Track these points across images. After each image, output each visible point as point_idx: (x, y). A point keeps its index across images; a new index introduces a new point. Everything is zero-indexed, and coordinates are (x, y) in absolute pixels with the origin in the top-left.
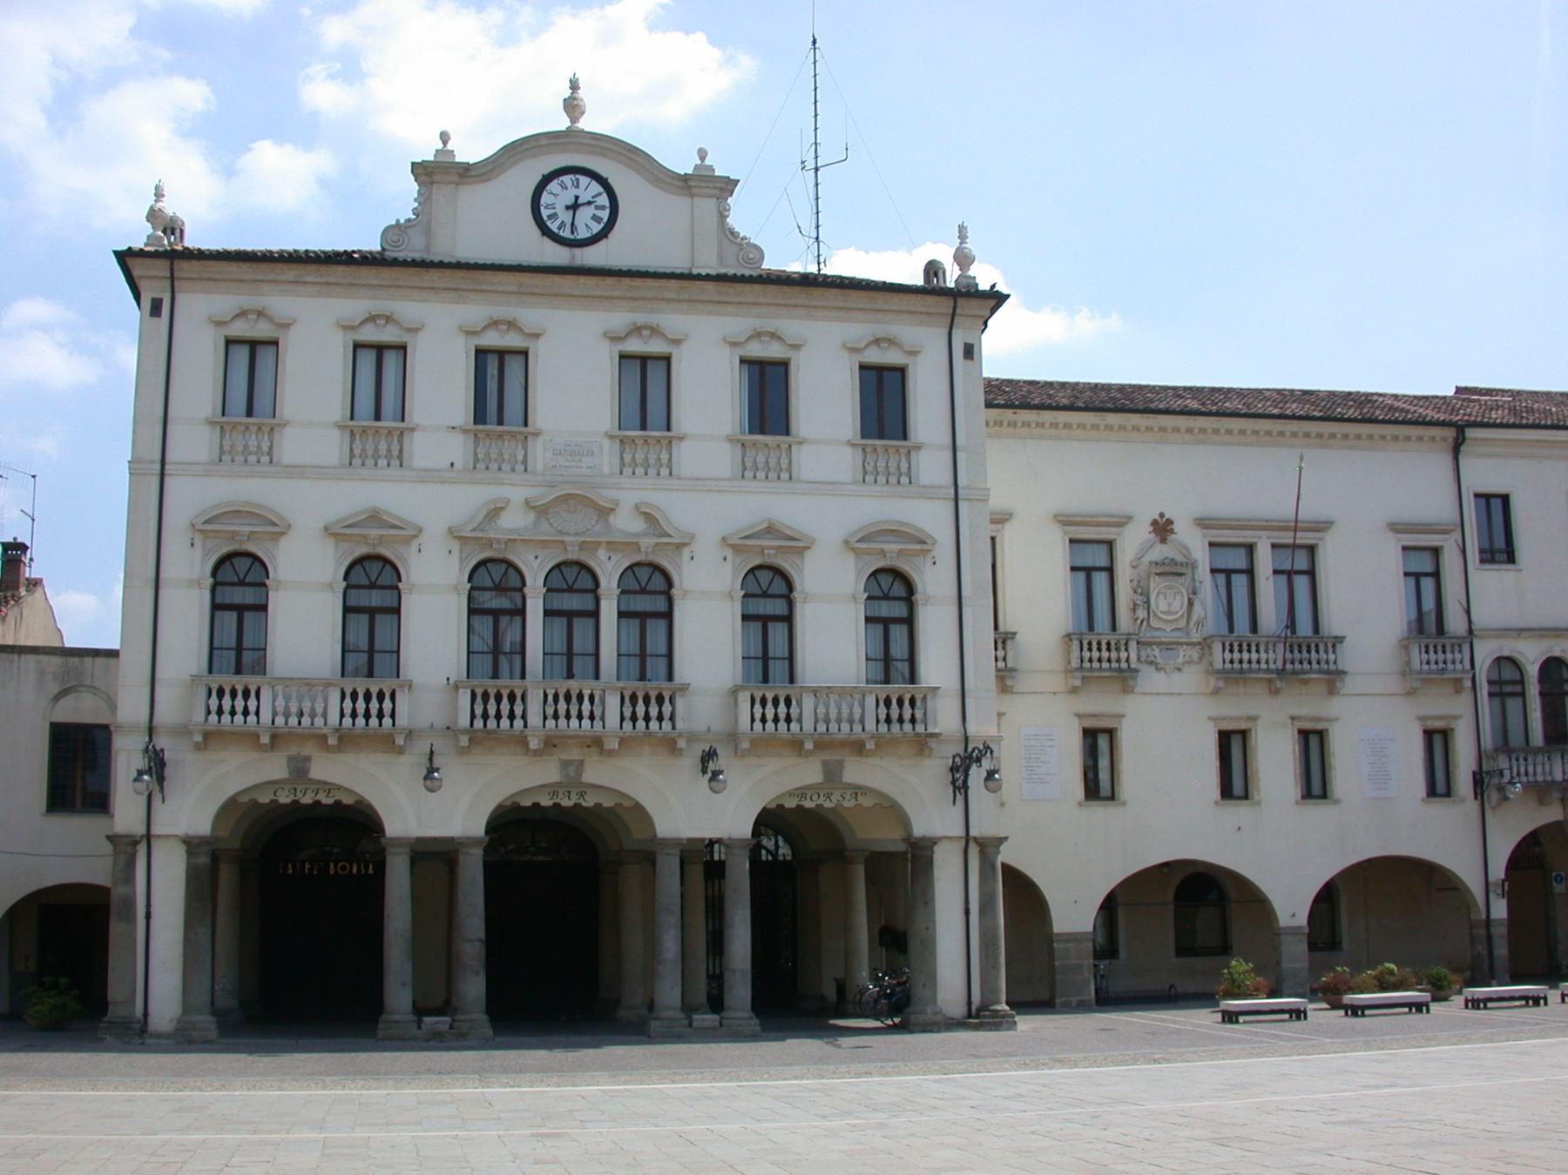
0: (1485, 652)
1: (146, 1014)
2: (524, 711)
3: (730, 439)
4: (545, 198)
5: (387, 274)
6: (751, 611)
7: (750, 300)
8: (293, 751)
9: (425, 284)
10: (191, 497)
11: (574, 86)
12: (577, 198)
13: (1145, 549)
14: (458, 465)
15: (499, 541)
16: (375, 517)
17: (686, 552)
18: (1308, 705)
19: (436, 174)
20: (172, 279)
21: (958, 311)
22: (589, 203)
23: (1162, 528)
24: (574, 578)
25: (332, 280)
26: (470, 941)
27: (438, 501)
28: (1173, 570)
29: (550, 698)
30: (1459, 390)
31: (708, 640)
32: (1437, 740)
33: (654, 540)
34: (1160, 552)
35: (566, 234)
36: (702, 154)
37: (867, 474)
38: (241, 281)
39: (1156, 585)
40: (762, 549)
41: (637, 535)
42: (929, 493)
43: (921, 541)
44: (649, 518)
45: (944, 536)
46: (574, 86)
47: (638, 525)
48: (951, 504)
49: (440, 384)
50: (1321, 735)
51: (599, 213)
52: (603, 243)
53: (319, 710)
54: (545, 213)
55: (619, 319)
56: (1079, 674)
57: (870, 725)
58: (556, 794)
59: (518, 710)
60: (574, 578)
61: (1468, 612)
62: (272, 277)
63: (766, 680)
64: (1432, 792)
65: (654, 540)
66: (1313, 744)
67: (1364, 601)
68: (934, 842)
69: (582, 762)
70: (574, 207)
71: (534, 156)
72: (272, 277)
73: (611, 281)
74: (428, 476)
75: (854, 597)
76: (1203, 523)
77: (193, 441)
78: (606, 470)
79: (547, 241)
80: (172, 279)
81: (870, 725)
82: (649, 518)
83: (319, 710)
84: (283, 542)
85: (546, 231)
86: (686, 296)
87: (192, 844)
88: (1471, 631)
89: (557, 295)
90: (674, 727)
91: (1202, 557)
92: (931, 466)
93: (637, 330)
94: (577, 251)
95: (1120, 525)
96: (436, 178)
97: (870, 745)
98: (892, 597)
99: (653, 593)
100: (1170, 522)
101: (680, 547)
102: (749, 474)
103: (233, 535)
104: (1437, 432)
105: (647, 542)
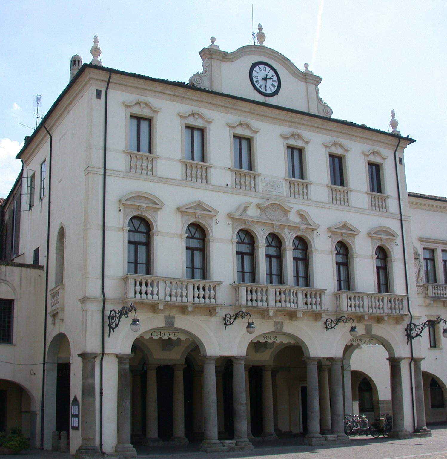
1: (101, 445)
2: (267, 298)
3: (181, 162)
4: (254, 74)
5: (191, 94)
6: (132, 239)
7: (333, 129)
8: (167, 313)
9: (214, 102)
10: (119, 187)
12: (267, 75)
14: (229, 186)
15: (248, 221)
16: (199, 205)
17: (315, 232)
19: (210, 54)
20: (109, 82)
21: (400, 145)
22: (271, 79)
24: (275, 240)
25: (177, 94)
26: (242, 404)
27: (223, 202)
29: (278, 293)
33: (306, 226)
35: (263, 90)
36: (213, 40)
38: (137, 88)
40: (342, 234)
41: (298, 223)
42: (392, 216)
44: (301, 215)
45: (399, 233)
48: (399, 222)
49: (221, 149)
51: (274, 83)
52: (251, 87)
53: (184, 294)
54: (255, 80)
55: (287, 130)
57: (386, 311)
58: (265, 337)
59: (265, 299)
62: (151, 88)
63: (136, 272)
65: (306, 226)
68: (401, 359)
69: (282, 322)
70: (265, 79)
71: (248, 55)
72: (151, 88)
73: (285, 113)
74: (218, 189)
75: (232, 241)
77: (117, 161)
78: (285, 194)
79: (255, 91)
80: (109, 82)
81: (386, 311)
82: (301, 215)
85: (255, 88)
86: (310, 124)
87: (120, 358)
89: (263, 116)
90: (392, 312)
93: (293, 135)
94: (267, 98)
96: (214, 56)
98: (383, 254)
99: (303, 245)
101: (313, 230)
102: (238, 187)
103: (138, 208)
105: (303, 227)
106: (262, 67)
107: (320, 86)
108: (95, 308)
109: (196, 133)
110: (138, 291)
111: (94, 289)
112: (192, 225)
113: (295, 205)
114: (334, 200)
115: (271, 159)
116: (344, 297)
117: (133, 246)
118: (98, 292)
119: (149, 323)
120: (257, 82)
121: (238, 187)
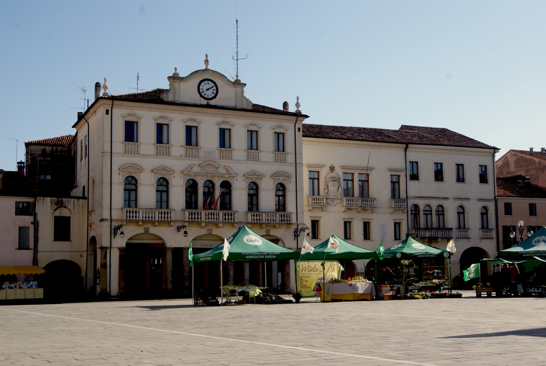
0: (411, 202)
3: (245, 150)
4: (201, 87)
11: (207, 56)
13: (328, 174)
14: (183, 155)
18: (367, 216)
19: (174, 78)
23: (332, 169)
24: (210, 186)
27: (179, 164)
28: (335, 180)
30: (403, 127)
31: (240, 200)
32: (397, 225)
34: (332, 175)
37: (276, 160)
39: (330, 183)
40: (253, 178)
41: (224, 174)
43: (288, 177)
46: (207, 56)
47: (224, 171)
49: (177, 135)
50: (369, 223)
52: (199, 96)
53: (153, 216)
54: (201, 91)
55: (219, 119)
56: (311, 206)
59: (199, 217)
60: (210, 186)
61: (407, 192)
64: (396, 239)
66: (366, 226)
67: (380, 188)
74: (176, 158)
76: (343, 167)
81: (278, 221)
83: (153, 216)
84: (142, 174)
85: (201, 96)
87: (121, 249)
88: (407, 198)
91: (342, 176)
92: (290, 158)
95: (322, 168)
97: (277, 226)
98: (281, 188)
99: (227, 185)
100: (334, 167)
102: (222, 158)
103: (130, 172)
104: (401, 145)
106: (206, 82)
107: (245, 89)
108: (107, 224)
109: (253, 135)
110: (128, 215)
111: (106, 215)
112: (279, 184)
113: (223, 163)
114: (249, 158)
115: (208, 137)
116: (250, 214)
117: (128, 192)
118: (109, 218)
119: (131, 231)
120: (203, 92)
121: (222, 158)
